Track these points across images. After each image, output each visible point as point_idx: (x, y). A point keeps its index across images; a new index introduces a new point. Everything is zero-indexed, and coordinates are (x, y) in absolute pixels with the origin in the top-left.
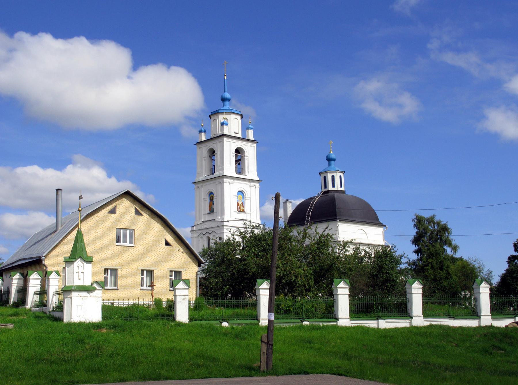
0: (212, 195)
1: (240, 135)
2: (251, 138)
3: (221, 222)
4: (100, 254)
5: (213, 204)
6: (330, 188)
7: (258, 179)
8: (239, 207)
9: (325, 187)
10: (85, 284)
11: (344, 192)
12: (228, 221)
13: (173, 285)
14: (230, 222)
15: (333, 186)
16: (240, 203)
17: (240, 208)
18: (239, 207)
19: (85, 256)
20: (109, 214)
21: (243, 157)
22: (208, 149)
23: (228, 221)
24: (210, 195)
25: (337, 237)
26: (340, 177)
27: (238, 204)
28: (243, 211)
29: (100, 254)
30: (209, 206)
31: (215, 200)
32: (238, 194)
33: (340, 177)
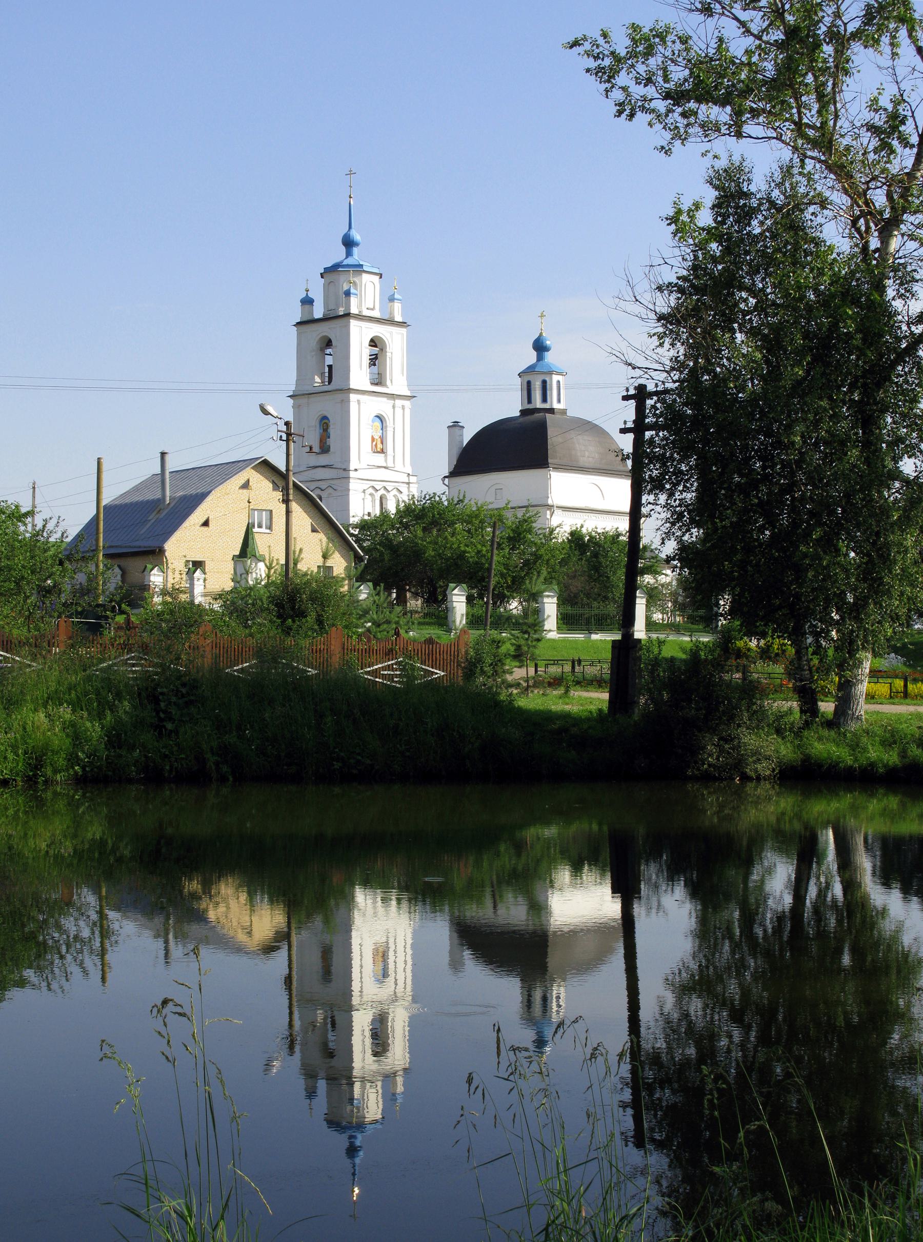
0: (326, 421)
1: (376, 314)
2: (398, 318)
3: (345, 470)
4: (230, 543)
5: (329, 437)
6: (538, 404)
7: (409, 394)
8: (374, 443)
9: (529, 401)
10: (637, 606)
11: (564, 412)
12: (356, 470)
13: (190, 574)
14: (359, 471)
15: (544, 400)
16: (376, 437)
17: (376, 445)
18: (374, 443)
19: (257, 554)
20: (241, 491)
21: (383, 350)
22: (319, 337)
23: (356, 470)
24: (321, 421)
25: (615, 920)
26: (559, 401)
27: (373, 439)
28: (382, 451)
29: (230, 543)
30: (321, 441)
31: (332, 431)
32: (373, 421)
33: (559, 401)
